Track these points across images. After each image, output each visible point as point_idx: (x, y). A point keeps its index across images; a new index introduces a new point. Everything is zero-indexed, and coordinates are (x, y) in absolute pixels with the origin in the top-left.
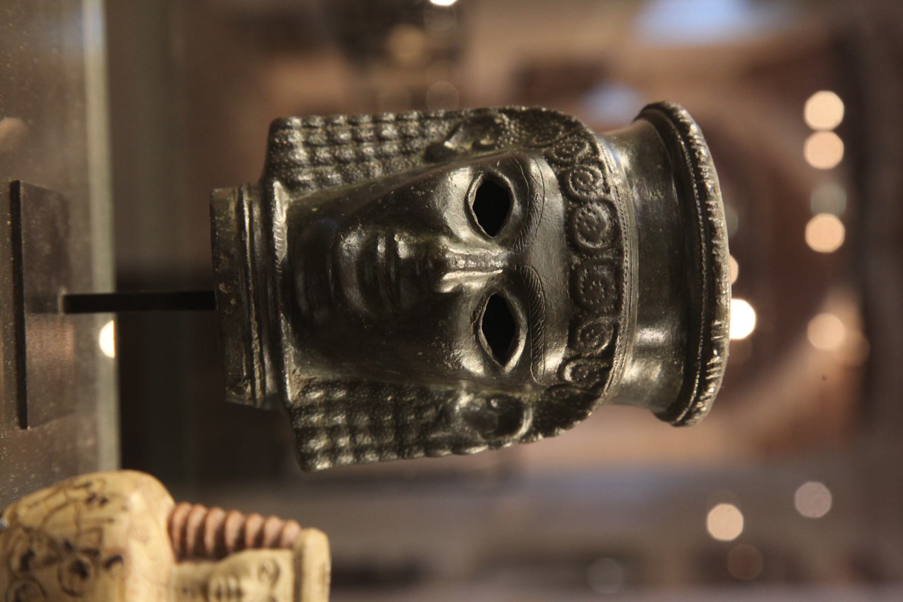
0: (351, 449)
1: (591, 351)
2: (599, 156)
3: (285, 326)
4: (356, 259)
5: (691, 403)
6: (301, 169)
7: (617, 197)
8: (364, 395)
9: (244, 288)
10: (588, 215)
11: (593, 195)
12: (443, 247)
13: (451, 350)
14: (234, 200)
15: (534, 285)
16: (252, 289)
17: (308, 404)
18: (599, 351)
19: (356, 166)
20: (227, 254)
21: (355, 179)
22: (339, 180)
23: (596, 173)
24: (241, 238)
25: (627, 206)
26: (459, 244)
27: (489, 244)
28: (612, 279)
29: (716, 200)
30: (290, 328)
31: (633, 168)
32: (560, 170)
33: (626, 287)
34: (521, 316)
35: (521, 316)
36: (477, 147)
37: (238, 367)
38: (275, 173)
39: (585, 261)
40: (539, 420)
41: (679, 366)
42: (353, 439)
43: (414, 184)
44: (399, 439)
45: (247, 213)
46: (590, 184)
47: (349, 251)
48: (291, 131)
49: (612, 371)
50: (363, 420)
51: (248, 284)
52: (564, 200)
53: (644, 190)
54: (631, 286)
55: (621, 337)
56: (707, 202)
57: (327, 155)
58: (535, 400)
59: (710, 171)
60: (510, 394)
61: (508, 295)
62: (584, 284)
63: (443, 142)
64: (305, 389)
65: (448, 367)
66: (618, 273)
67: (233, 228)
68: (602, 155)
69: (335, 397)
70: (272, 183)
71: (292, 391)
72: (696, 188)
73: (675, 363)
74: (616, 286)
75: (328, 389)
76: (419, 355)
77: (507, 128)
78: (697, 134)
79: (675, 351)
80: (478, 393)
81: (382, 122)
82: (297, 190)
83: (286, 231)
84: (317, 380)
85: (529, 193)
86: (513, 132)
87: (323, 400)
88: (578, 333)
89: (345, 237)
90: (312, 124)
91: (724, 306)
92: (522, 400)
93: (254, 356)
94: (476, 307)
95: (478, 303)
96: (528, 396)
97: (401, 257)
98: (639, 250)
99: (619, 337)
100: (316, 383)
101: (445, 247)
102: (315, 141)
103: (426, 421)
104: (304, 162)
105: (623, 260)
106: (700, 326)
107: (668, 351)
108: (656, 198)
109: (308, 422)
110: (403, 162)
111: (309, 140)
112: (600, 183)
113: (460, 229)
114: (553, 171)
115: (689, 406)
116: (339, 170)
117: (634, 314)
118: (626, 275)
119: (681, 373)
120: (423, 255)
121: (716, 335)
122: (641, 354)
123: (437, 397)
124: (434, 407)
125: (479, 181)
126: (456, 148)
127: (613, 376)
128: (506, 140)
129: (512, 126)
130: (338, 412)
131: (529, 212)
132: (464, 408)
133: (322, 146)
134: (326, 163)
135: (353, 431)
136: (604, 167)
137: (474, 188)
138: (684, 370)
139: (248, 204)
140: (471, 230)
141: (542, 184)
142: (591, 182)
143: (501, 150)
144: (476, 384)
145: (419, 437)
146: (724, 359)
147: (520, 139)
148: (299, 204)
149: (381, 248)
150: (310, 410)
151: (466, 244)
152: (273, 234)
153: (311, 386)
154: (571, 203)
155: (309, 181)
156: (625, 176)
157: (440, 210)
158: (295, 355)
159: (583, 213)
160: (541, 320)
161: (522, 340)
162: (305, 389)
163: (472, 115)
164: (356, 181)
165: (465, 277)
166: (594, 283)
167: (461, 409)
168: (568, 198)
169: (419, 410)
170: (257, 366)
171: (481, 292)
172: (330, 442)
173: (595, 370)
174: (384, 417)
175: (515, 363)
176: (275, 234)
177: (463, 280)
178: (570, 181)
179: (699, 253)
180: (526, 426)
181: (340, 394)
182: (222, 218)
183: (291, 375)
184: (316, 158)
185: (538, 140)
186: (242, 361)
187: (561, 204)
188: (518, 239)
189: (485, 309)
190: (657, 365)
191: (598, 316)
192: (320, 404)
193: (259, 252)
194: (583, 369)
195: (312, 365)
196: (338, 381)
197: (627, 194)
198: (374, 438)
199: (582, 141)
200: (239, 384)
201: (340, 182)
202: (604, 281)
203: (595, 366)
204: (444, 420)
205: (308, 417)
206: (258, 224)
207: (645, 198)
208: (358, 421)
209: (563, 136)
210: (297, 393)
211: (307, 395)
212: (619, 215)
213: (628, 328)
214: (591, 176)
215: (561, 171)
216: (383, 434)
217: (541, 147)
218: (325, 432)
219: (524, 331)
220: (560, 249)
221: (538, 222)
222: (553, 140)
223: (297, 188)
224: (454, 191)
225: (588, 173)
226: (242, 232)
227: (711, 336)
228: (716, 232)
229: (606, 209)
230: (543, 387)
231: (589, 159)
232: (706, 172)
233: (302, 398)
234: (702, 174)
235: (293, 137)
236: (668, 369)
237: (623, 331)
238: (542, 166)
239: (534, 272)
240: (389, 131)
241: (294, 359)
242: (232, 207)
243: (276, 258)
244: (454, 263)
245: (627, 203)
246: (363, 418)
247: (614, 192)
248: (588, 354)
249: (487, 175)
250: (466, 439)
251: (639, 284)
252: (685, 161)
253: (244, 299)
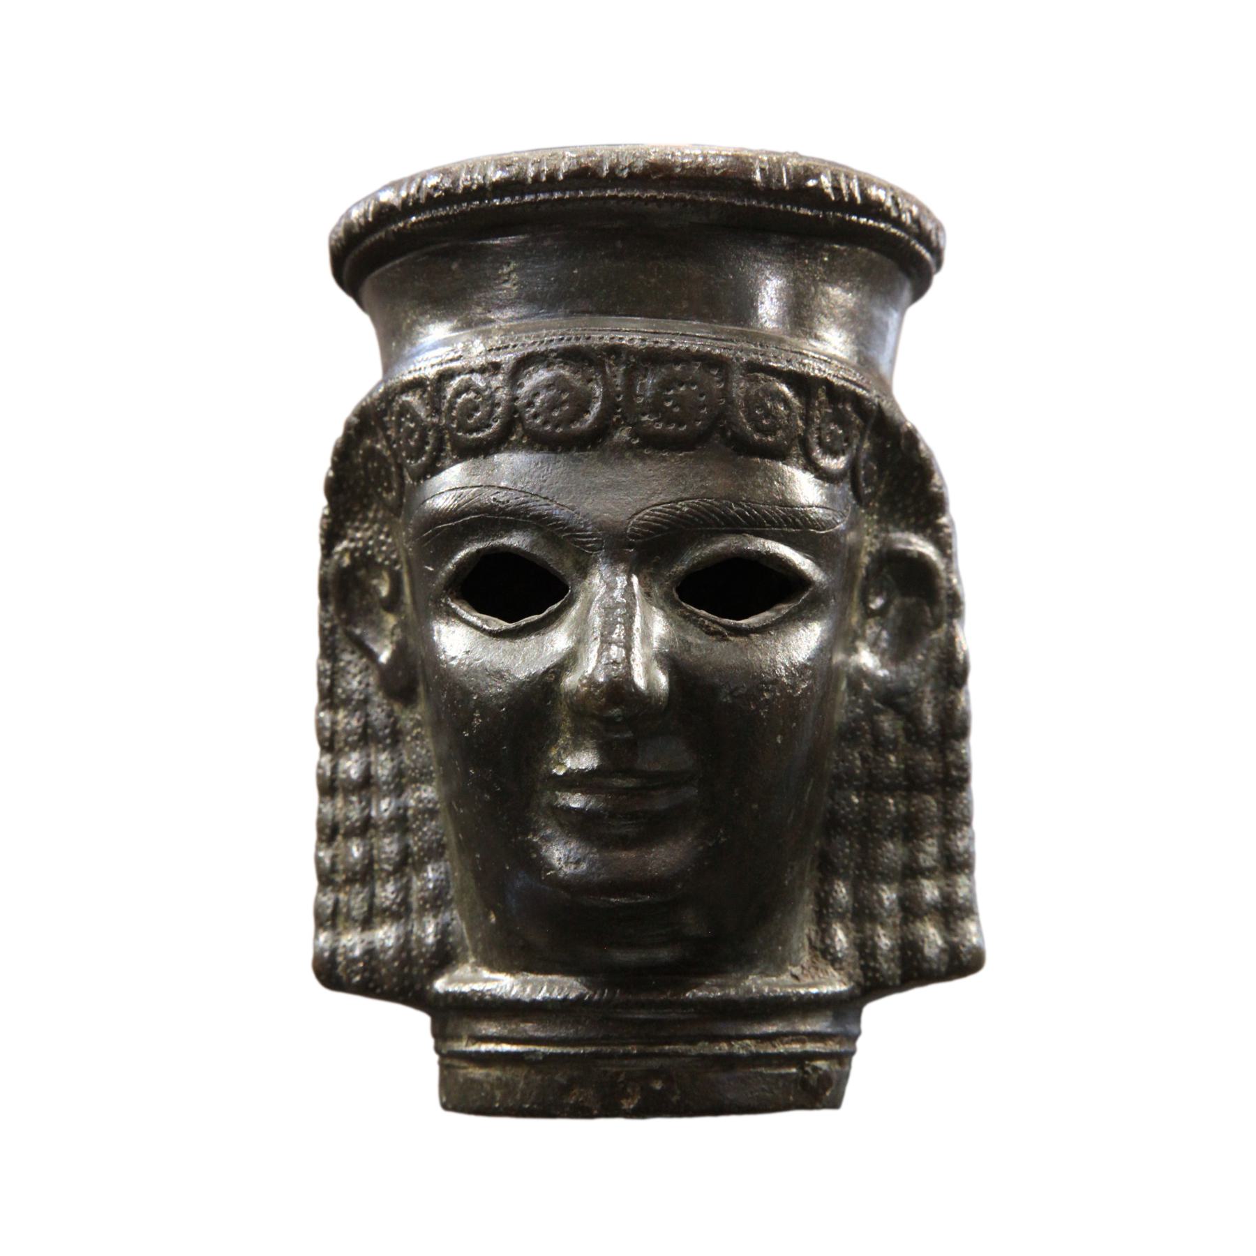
0: (947, 877)
1: (795, 417)
2: (427, 379)
3: (708, 991)
4: (595, 850)
5: (903, 235)
6: (414, 938)
7: (508, 350)
8: (845, 848)
9: (633, 1062)
10: (540, 406)
11: (502, 395)
12: (583, 685)
13: (776, 681)
14: (465, 1068)
15: (664, 517)
16: (635, 1047)
17: (857, 953)
18: (796, 402)
19: (415, 835)
21: (438, 836)
22: (440, 867)
23: (460, 385)
24: (537, 1062)
26: (579, 654)
27: (581, 597)
28: (663, 370)
29: (526, 163)
30: (714, 980)
31: (455, 315)
32: (450, 453)
33: (681, 344)
34: (721, 545)
35: (721, 545)
36: (392, 604)
37: (781, 1084)
38: (418, 987)
39: (625, 418)
40: (912, 520)
41: (833, 253)
42: (927, 873)
44: (933, 785)
45: (491, 1047)
46: (481, 399)
47: (578, 862)
48: (341, 950)
49: (834, 380)
51: (627, 1056)
52: (507, 449)
54: (678, 334)
55: (772, 359)
56: (530, 180)
57: (390, 887)
60: (863, 572)
61: (680, 568)
62: (668, 423)
63: (379, 666)
64: (829, 957)
65: (808, 688)
66: (653, 358)
69: (847, 902)
70: (437, 993)
71: (831, 984)
72: (502, 199)
73: (826, 259)
74: (677, 363)
75: (831, 915)
76: (782, 741)
79: (806, 258)
80: (855, 632)
82: (454, 948)
83: (531, 976)
84: (813, 935)
85: (490, 515)
86: (369, 533)
87: (851, 925)
88: (760, 440)
89: (551, 867)
90: (329, 911)
91: (727, 161)
92: (873, 549)
93: (762, 1051)
94: (698, 630)
95: (692, 626)
96: (867, 538)
97: (596, 765)
98: (611, 315)
99: (771, 364)
100: (819, 937)
101: (585, 681)
102: (362, 907)
103: (900, 732)
104: (401, 931)
105: (628, 346)
106: (761, 209)
107: (802, 271)
108: (514, 276)
109: (891, 956)
110: (413, 744)
111: (361, 917)
112: (478, 380)
113: (550, 649)
114: (450, 466)
115: (907, 237)
116: (419, 867)
117: (731, 333)
118: (657, 342)
119: (845, 250)
120: (594, 723)
121: (780, 180)
122: (806, 322)
124: (876, 717)
125: (460, 607)
126: (392, 643)
127: (844, 379)
129: (359, 535)
130: (875, 897)
131: (527, 519)
132: (881, 661)
133: (373, 895)
134: (405, 889)
135: (911, 872)
136: (450, 369)
137: (474, 618)
138: (840, 243)
139: (474, 1044)
140: (552, 630)
141: (475, 489)
142: (475, 398)
143: (403, 559)
144: (843, 638)
145: (930, 748)
147: (383, 522)
148: (480, 947)
149: (576, 801)
150: (867, 951)
151: (581, 641)
152: (534, 1002)
153: (823, 947)
154: (514, 438)
155: (437, 924)
156: (469, 331)
157: (513, 685)
158: (764, 973)
159: (535, 416)
160: (732, 508)
161: (766, 546)
162: (829, 957)
164: (443, 835)
166: (669, 404)
167: (883, 666)
168: (504, 443)
169: (879, 743)
170: (781, 1046)
171: (672, 618)
172: (929, 916)
173: (829, 411)
174: (889, 812)
175: (808, 561)
176: (533, 997)
177: (647, 650)
178: (472, 437)
179: (624, 203)
180: (923, 547)
181: (841, 892)
182: (498, 1094)
183: (802, 983)
184: (394, 907)
185: (389, 490)
186: (771, 1075)
187: (515, 456)
188: (576, 543)
189: (703, 612)
190: (828, 293)
191: (731, 402)
192: (857, 931)
193: (567, 1028)
194: (827, 434)
195: (785, 942)
196: (817, 895)
197: (503, 330)
198: (927, 834)
199: (396, 407)
200: (811, 1082)
201: (443, 866)
202: (665, 385)
203: (824, 410)
204: (902, 700)
205: (882, 955)
206: (514, 1027)
207: (513, 296)
208: (896, 862)
209: (384, 443)
210: (836, 974)
211: (840, 955)
212: (542, 348)
214: (464, 396)
215: (453, 450)
216: (921, 815)
217: (402, 484)
218: (911, 925)
219: (750, 542)
220: (600, 464)
221: (548, 502)
222: (391, 460)
223: (449, 948)
224: (477, 656)
225: (459, 400)
227: (782, 189)
228: (587, 169)
229: (529, 372)
230: (854, 511)
231: (431, 397)
232: (471, 179)
233: (844, 964)
234: (474, 187)
235: (352, 949)
236: (836, 274)
237: (761, 355)
238: (440, 487)
239: (640, 515)
241: (772, 976)
242: (477, 1073)
243: (580, 998)
244: (615, 667)
245: (520, 332)
246: (889, 851)
247: (498, 355)
248: (800, 423)
249: (450, 590)
250: (939, 659)
251: (673, 319)
252: (447, 217)
253: (654, 1063)
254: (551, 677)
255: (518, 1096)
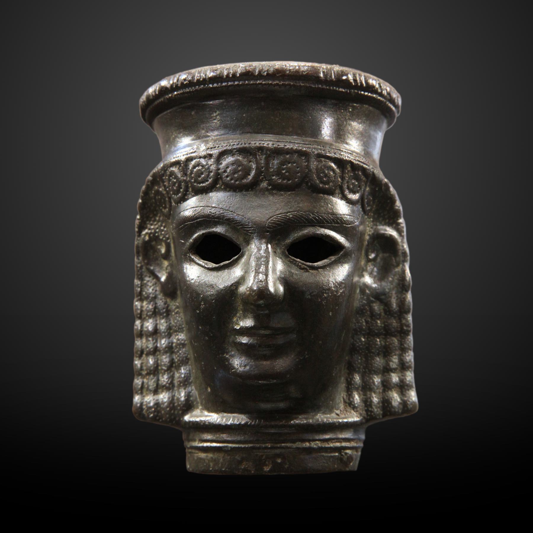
0: (402, 372)
1: (337, 177)
2: (181, 161)
3: (300, 420)
4: (252, 361)
5: (383, 100)
6: (176, 398)
7: (216, 148)
8: (358, 360)
9: (269, 451)
10: (229, 172)
11: (213, 168)
12: (248, 291)
13: (329, 289)
14: (197, 453)
15: (282, 219)
16: (269, 444)
17: (364, 405)
18: (338, 171)
19: (176, 354)
21: (186, 355)
22: (187, 368)
23: (195, 163)
24: (228, 451)
26: (246, 278)
27: (247, 253)
28: (281, 157)
29: (223, 69)
30: (303, 416)
31: (193, 134)
32: (191, 192)
33: (289, 146)
34: (306, 231)
35: (306, 231)
36: (167, 256)
37: (331, 460)
38: (177, 419)
39: (265, 177)
40: (387, 221)
41: (353, 107)
42: (393, 371)
44: (396, 333)
45: (208, 444)
46: (204, 169)
47: (245, 366)
48: (145, 403)
49: (354, 161)
51: (266, 448)
52: (215, 191)
53: (211, 127)
54: (288, 142)
55: (328, 153)
56: (225, 77)
57: (166, 377)
58: (372, 224)
59: (199, 73)
60: (366, 243)
61: (289, 241)
62: (284, 179)
63: (161, 283)
64: (352, 406)
66: (277, 152)
67: (220, 456)
70: (186, 422)
71: (353, 418)
72: (213, 85)
73: (350, 110)
74: (287, 154)
76: (332, 315)
77: (153, 231)
78: (169, 81)
79: (342, 109)
80: (363, 268)
81: (141, 331)
82: (193, 402)
83: (225, 414)
84: (345, 397)
85: (208, 218)
86: (157, 226)
87: (361, 393)
88: (323, 187)
89: (234, 368)
90: (140, 387)
92: (371, 233)
93: (323, 446)
94: (296, 267)
95: (294, 265)
96: (368, 228)
98: (259, 134)
99: (327, 154)
100: (348, 398)
101: (248, 289)
102: (153, 385)
103: (382, 311)
104: (170, 395)
105: (267, 147)
106: (323, 89)
107: (340, 115)
108: (218, 117)
109: (378, 406)
110: (175, 316)
111: (153, 389)
112: (203, 161)
113: (233, 275)
114: (191, 198)
115: (385, 101)
116: (178, 368)
117: (310, 141)
118: (279, 145)
119: (359, 106)
120: (252, 307)
121: (331, 76)
122: (342, 137)
123: (364, 301)
124: (372, 304)
125: (195, 258)
126: (166, 273)
127: (358, 161)
128: (163, 233)
129: (152, 227)
130: (371, 381)
131: (224, 220)
132: (374, 280)
133: (158, 380)
134: (172, 377)
135: (387, 370)
136: (191, 157)
137: (201, 262)
138: (357, 103)
139: (201, 443)
140: (234, 267)
141: (201, 208)
142: (202, 169)
143: (171, 237)
144: (358, 271)
145: (395, 318)
146: (350, 71)
147: (163, 222)
148: (204, 402)
149: (244, 340)
150: (368, 403)
151: (246, 272)
152: (227, 425)
153: (349, 402)
154: (218, 186)
155: (185, 392)
156: (199, 140)
157: (218, 291)
158: (324, 413)
159: (227, 176)
160: (311, 216)
161: (325, 232)
162: (352, 406)
163: (141, 258)
164: (188, 354)
165: (273, 275)
166: (284, 172)
167: (375, 283)
168: (214, 188)
169: (373, 315)
170: (332, 444)
171: (285, 262)
172: (394, 389)
173: (352, 174)
174: (377, 345)
175: (343, 238)
176: (226, 423)
177: (275, 276)
178: (200, 185)
179: (265, 86)
180: (392, 232)
181: (357, 378)
182: (211, 464)
183: (340, 417)
185: (165, 208)
186: (327, 456)
187: (219, 193)
188: (244, 230)
189: (298, 260)
190: (351, 124)
191: (310, 170)
192: (364, 395)
193: (240, 436)
195: (333, 400)
196: (347, 380)
197: (214, 140)
198: (393, 354)
199: (168, 173)
200: (344, 459)
201: (188, 368)
202: (282, 163)
203: (350, 174)
204: (383, 297)
205: (374, 405)
206: (218, 436)
208: (380, 366)
209: (163, 188)
210: (355, 413)
211: (356, 405)
212: (230, 148)
214: (197, 168)
216: (391, 346)
217: (171, 206)
218: (387, 393)
219: (318, 230)
220: (254, 197)
221: (232, 213)
222: (166, 195)
223: (190, 402)
224: (203, 278)
225: (195, 170)
226: (223, 449)
227: (332, 80)
228: (249, 72)
229: (225, 158)
231: (183, 169)
232: (200, 76)
233: (358, 409)
234: (201, 79)
235: (149, 403)
236: (355, 116)
237: (323, 151)
238: (187, 207)
239: (272, 219)
240: (149, 325)
241: (328, 414)
242: (203, 455)
243: (246, 424)
244: (261, 283)
245: (221, 141)
246: (377, 361)
247: (212, 151)
248: (339, 179)
249: (191, 251)
250: (398, 280)
251: (286, 135)
252: (190, 92)
253: (278, 451)
254: (234, 287)
255: (220, 465)
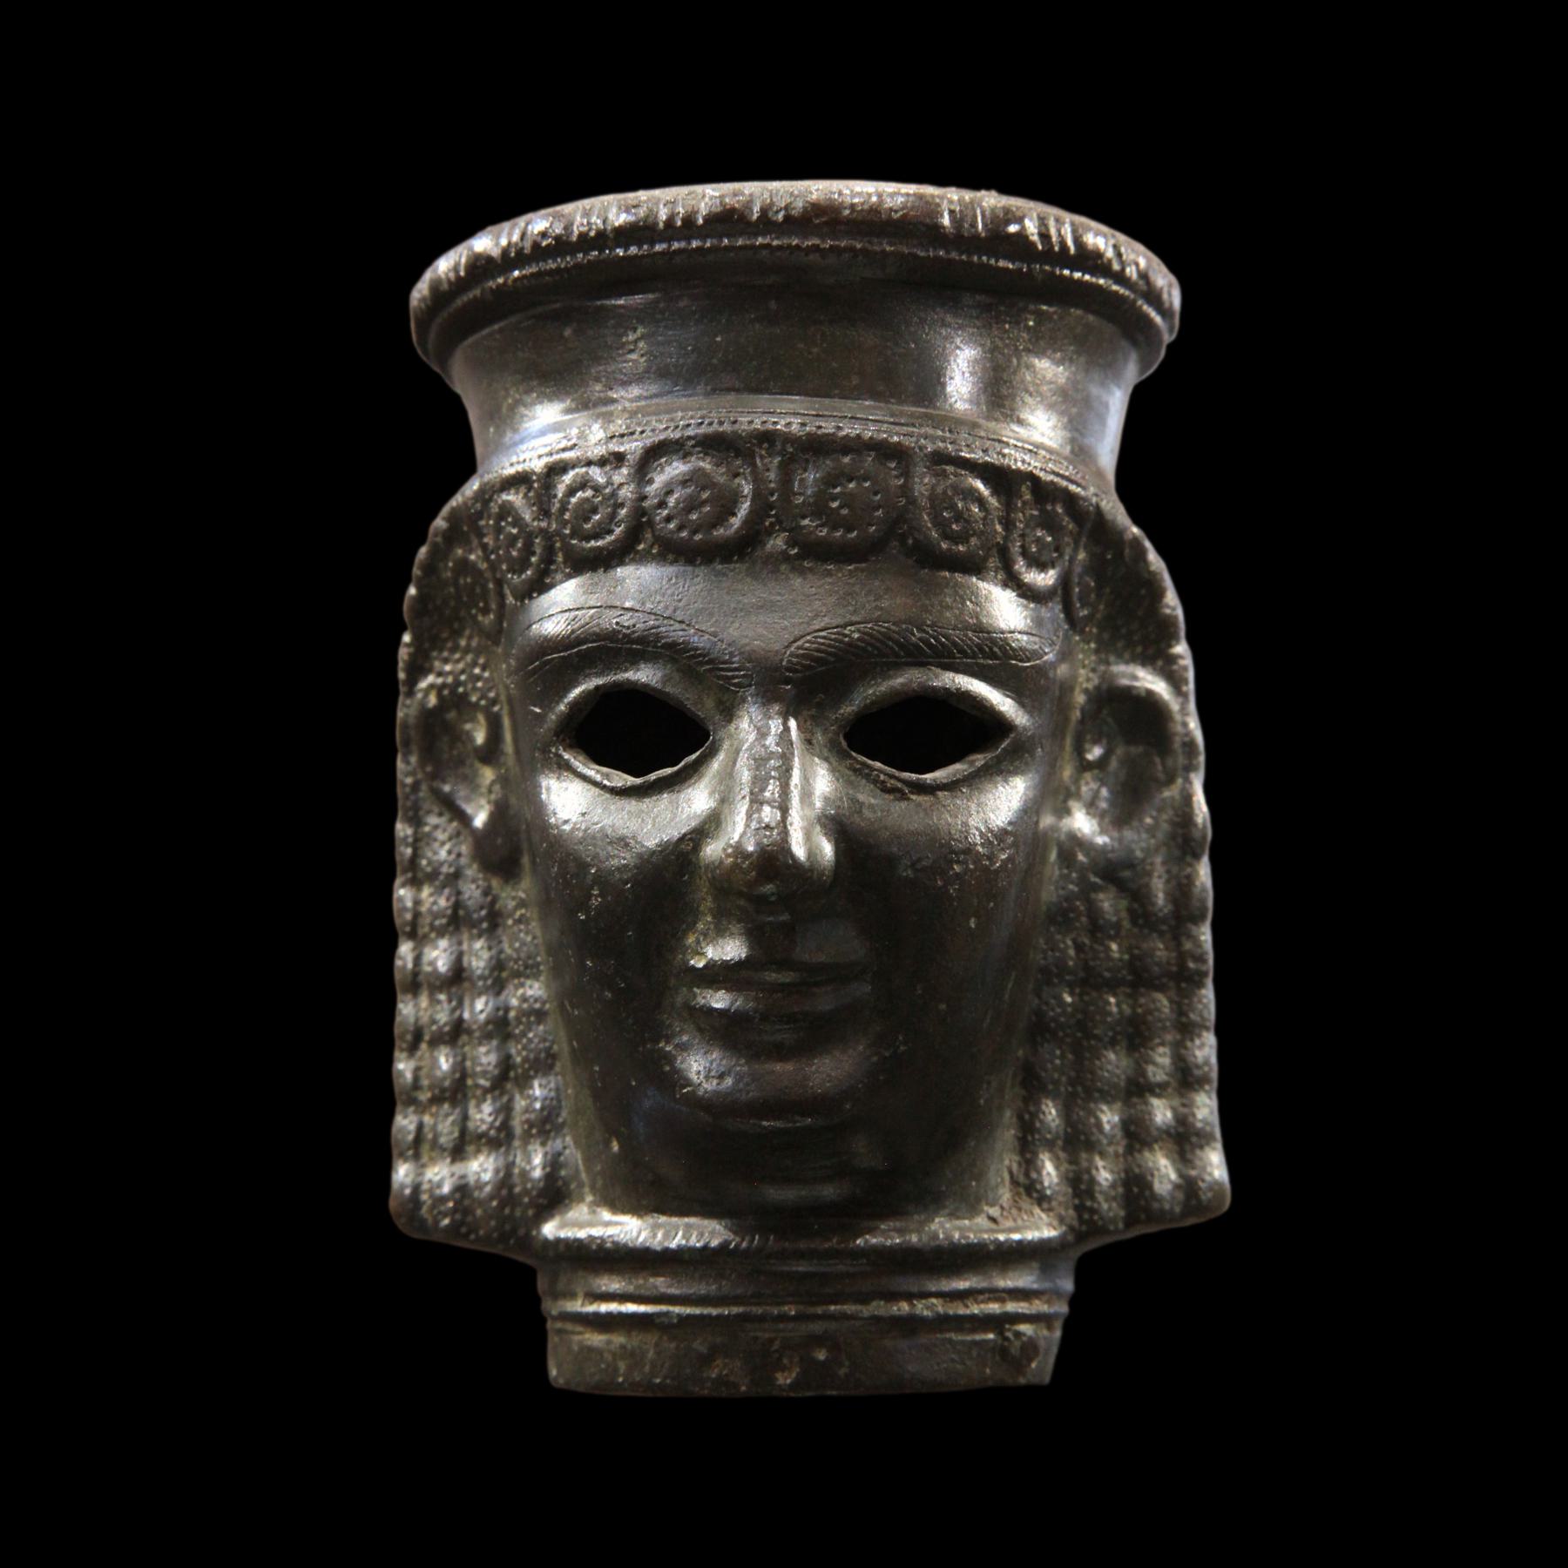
0: (1182, 1095)
1: (992, 520)
2: (533, 473)
3: (884, 1237)
4: (743, 1061)
5: (1127, 293)
6: (516, 1171)
7: (635, 437)
8: (1055, 1059)
9: (791, 1325)
10: (674, 507)
11: (626, 493)
12: (728, 856)
13: (969, 850)
14: (580, 1333)
15: (829, 646)
16: (792, 1307)
17: (1070, 1190)
18: (994, 502)
19: (518, 1042)
20: (706, 1360)
22: (549, 1082)
23: (574, 481)
24: (671, 1326)
25: (659, 414)
26: (723, 817)
27: (726, 745)
28: (828, 462)
29: (657, 204)
30: (891, 1224)
31: (568, 394)
32: (562, 566)
33: (850, 430)
34: (900, 680)
35: (900, 680)
36: (490, 754)
37: (974, 1353)
38: (522, 1232)
39: (780, 522)
40: (1139, 649)
41: (1040, 316)
42: (1157, 1090)
43: (572, 913)
44: (1165, 980)
45: (613, 1307)
46: (600, 498)
47: (721, 1077)
48: (425, 1187)
49: (1042, 474)
50: (1114, 1063)
51: (783, 1318)
52: (633, 561)
54: (846, 417)
55: (964, 449)
56: (661, 225)
57: (487, 1108)
59: (587, 214)
60: (1077, 714)
61: (849, 709)
62: (834, 528)
63: (473, 831)
64: (1035, 1195)
66: (816, 447)
67: (647, 1342)
68: (533, 466)
69: (1057, 1126)
70: (546, 1240)
71: (1038, 1228)
72: (626, 249)
73: (1031, 323)
74: (845, 453)
76: (976, 925)
77: (450, 680)
78: (498, 237)
79: (1006, 322)
80: (1067, 789)
81: (416, 973)
82: (566, 1184)
83: (663, 1219)
84: (1015, 1167)
85: (612, 642)
86: (461, 666)
87: (1062, 1155)
88: (949, 550)
89: (688, 1083)
90: (411, 1137)
92: (1090, 686)
93: (951, 1312)
94: (872, 786)
95: (864, 781)
96: (1082, 671)
98: (763, 394)
99: (963, 454)
100: (1023, 1170)
101: (730, 850)
102: (451, 1133)
103: (1124, 914)
104: (501, 1162)
105: (785, 432)
106: (950, 261)
107: (1001, 339)
108: (641, 344)
109: (1113, 1193)
110: (515, 928)
111: (451, 1145)
112: (597, 475)
113: (687, 810)
114: (562, 582)
115: (1132, 296)
116: (524, 1082)
117: (912, 415)
118: (820, 427)
119: (1055, 313)
120: (742, 902)
121: (974, 225)
122: (1006, 403)
123: (1071, 887)
124: (1093, 896)
125: (575, 758)
126: (489, 802)
127: (1054, 473)
129: (448, 668)
130: (1092, 1120)
131: (658, 647)
132: (1100, 825)
133: (465, 1117)
134: (506, 1110)
135: (1137, 1089)
136: (561, 461)
137: (592, 771)
138: (1049, 304)
139: (591, 1303)
140: (689, 786)
141: (593, 611)
142: (593, 496)
143: (503, 698)
144: (1053, 796)
145: (1161, 934)
146: (1031, 209)
147: (478, 652)
148: (600, 1183)
149: (719, 1000)
150: (1083, 1187)
151: (725, 800)
152: (667, 1251)
153: (1027, 1182)
154: (641, 547)
155: (546, 1154)
156: (586, 413)
157: (640, 856)
158: (953, 1215)
159: (668, 519)
160: (914, 635)
161: (957, 681)
162: (1035, 1195)
164: (553, 1042)
165: (802, 809)
166: (835, 505)
167: (1103, 832)
168: (629, 553)
169: (1098, 928)
170: (976, 1306)
171: (839, 771)
172: (1160, 1143)
173: (1036, 513)
174: (1110, 1014)
175: (1009, 701)
176: (666, 1244)
177: (808, 812)
178: (589, 545)
179: (779, 254)
180: (1153, 683)
181: (1050, 1113)
182: (622, 1366)
183: (1001, 1227)
184: (492, 1132)
185: (485, 611)
186: (963, 1343)
187: (643, 569)
188: (719, 678)
189: (878, 765)
190: (1033, 366)
191: (912, 501)
192: (1070, 1163)
193: (707, 1283)
194: (1033, 542)
195: (980, 1176)
196: (1020, 1117)
197: (628, 411)
198: (1157, 1041)
199: (494, 509)
200: (1013, 1351)
201: (553, 1081)
202: (831, 481)
203: (1028, 512)
204: (1127, 874)
205: (1101, 1192)
206: (641, 1282)
208: (1118, 1077)
209: (480, 553)
210: (1043, 1216)
211: (1048, 1192)
212: (677, 435)
213: (943, 431)
214: (579, 494)
215: (565, 562)
216: (1150, 1018)
217: (502, 605)
218: (1137, 1155)
219: (937, 677)
220: (749, 580)
221: (684, 626)
222: (488, 575)
223: (560, 1183)
224: (596, 819)
225: (573, 500)
226: (657, 1321)
227: (976, 237)
228: (733, 210)
229: (661, 464)
231: (538, 496)
232: (589, 223)
233: (1054, 1203)
234: (592, 234)
235: (439, 1185)
236: (1043, 342)
237: (951, 443)
238: (549, 608)
239: (799, 643)
240: (439, 956)
241: (964, 1218)
242: (596, 1339)
243: (724, 1246)
244: (768, 833)
245: (649, 414)
246: (1109, 1062)
247: (622, 444)
248: (999, 528)
249: (561, 737)
250: (1172, 823)
251: (840, 398)
252: (558, 270)
253: (817, 1328)
254: (688, 845)
255: (647, 1369)
